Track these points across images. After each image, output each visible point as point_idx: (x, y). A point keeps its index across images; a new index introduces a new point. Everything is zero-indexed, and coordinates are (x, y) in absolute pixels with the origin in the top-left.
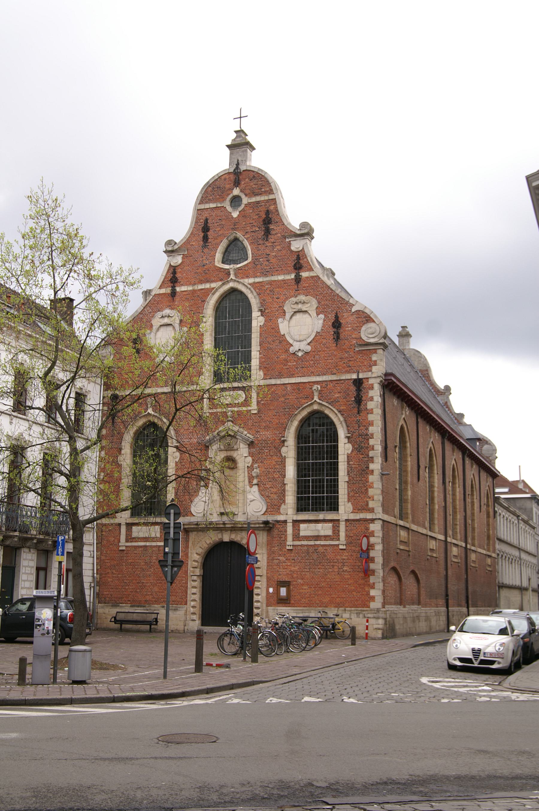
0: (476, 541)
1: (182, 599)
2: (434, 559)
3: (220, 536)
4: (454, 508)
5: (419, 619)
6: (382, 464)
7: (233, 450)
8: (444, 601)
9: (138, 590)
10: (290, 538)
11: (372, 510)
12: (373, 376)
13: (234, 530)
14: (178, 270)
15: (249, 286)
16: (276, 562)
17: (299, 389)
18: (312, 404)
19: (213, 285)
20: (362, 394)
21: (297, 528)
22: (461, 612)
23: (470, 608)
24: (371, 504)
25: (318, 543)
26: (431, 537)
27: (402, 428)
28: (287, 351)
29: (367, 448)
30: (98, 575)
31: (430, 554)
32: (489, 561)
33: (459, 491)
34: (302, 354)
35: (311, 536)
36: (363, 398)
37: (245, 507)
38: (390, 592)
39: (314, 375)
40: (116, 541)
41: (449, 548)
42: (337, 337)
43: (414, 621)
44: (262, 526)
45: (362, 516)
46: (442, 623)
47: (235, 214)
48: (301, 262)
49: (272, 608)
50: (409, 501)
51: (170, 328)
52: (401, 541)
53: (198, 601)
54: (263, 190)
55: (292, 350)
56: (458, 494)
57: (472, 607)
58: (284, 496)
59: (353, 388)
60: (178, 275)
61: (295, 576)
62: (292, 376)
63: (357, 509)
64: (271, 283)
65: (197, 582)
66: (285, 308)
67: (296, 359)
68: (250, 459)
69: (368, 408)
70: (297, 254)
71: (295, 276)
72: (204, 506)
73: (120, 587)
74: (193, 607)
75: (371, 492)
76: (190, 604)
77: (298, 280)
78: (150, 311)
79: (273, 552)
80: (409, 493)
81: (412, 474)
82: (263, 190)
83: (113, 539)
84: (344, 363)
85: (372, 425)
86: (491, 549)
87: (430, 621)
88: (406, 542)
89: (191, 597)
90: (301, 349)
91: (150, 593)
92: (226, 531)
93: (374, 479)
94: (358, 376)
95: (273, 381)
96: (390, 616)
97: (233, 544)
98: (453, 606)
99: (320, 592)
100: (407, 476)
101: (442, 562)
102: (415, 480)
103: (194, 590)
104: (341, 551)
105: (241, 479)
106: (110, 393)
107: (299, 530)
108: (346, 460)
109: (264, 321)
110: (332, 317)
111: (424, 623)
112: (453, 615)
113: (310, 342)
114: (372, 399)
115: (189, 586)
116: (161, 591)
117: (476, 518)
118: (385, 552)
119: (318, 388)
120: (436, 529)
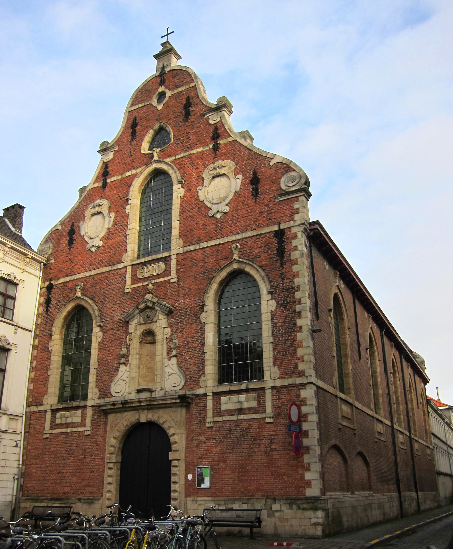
0: (417, 432)
1: (99, 490)
2: (382, 443)
3: (137, 417)
4: (397, 399)
5: (371, 507)
6: (312, 321)
7: (151, 323)
8: (395, 486)
9: (58, 482)
10: (210, 414)
11: (302, 374)
12: (296, 224)
13: (152, 409)
14: (110, 165)
15: (170, 163)
16: (195, 442)
17: (218, 251)
18: (231, 263)
19: (139, 170)
20: (284, 245)
21: (218, 401)
22: (411, 497)
23: (419, 493)
24: (301, 366)
25: (241, 417)
26: (377, 420)
27: (336, 296)
28: (206, 215)
29: (293, 302)
30: (24, 467)
31: (378, 437)
32: (428, 451)
33: (399, 384)
34: (221, 215)
35: (233, 410)
36: (286, 250)
37: (163, 382)
38: (333, 475)
39: (233, 234)
40: (42, 429)
41: (395, 434)
42: (256, 193)
43: (365, 510)
44: (178, 401)
45: (290, 381)
46: (395, 509)
47: (160, 107)
48: (219, 132)
49: (191, 498)
50: (351, 375)
51: (99, 217)
52: (343, 416)
53: (114, 492)
54: (185, 82)
55: (210, 213)
56: (399, 387)
57: (420, 491)
58: (204, 366)
59: (274, 241)
60: (109, 169)
61: (216, 458)
62: (211, 239)
63: (284, 375)
64: (190, 156)
65: (113, 471)
66: (203, 176)
67: (215, 222)
68: (168, 330)
69: (292, 258)
70: (215, 125)
71: (214, 145)
72: (124, 385)
73: (42, 479)
74: (108, 499)
75: (300, 352)
76: (106, 495)
77: (216, 148)
78: (85, 204)
79: (193, 432)
80: (350, 367)
81: (351, 348)
82: (185, 82)
83: (39, 427)
84: (264, 217)
85: (298, 276)
86: (429, 442)
87: (384, 508)
88: (350, 419)
89: (106, 488)
90: (220, 210)
91: (68, 484)
92: (143, 410)
93: (303, 336)
94: (279, 227)
95: (192, 248)
96: (333, 506)
97: (151, 424)
98: (404, 491)
99: (245, 478)
100: (346, 349)
101: (390, 447)
102: (356, 358)
103: (110, 480)
104: (268, 426)
105: (158, 353)
106: (47, 283)
107: (220, 404)
108: (270, 318)
109: (184, 192)
110: (250, 175)
111: (376, 510)
112: (405, 501)
113: (229, 203)
114: (296, 248)
115: (105, 476)
116: (79, 481)
117: (415, 413)
118: (322, 425)
119: (237, 246)
120: (382, 412)
